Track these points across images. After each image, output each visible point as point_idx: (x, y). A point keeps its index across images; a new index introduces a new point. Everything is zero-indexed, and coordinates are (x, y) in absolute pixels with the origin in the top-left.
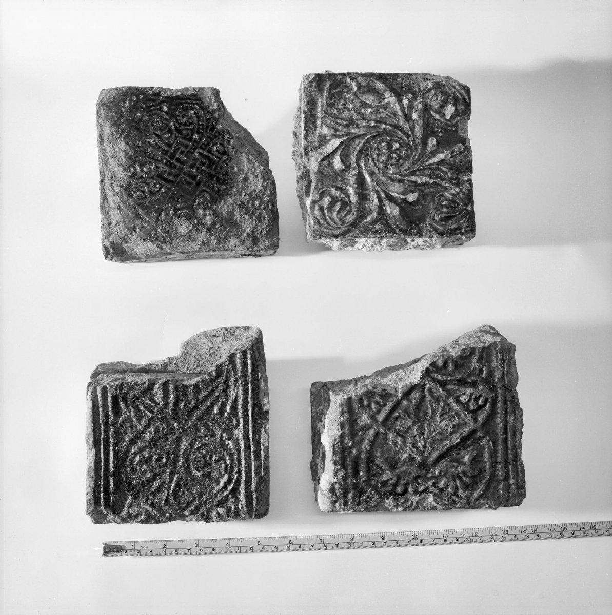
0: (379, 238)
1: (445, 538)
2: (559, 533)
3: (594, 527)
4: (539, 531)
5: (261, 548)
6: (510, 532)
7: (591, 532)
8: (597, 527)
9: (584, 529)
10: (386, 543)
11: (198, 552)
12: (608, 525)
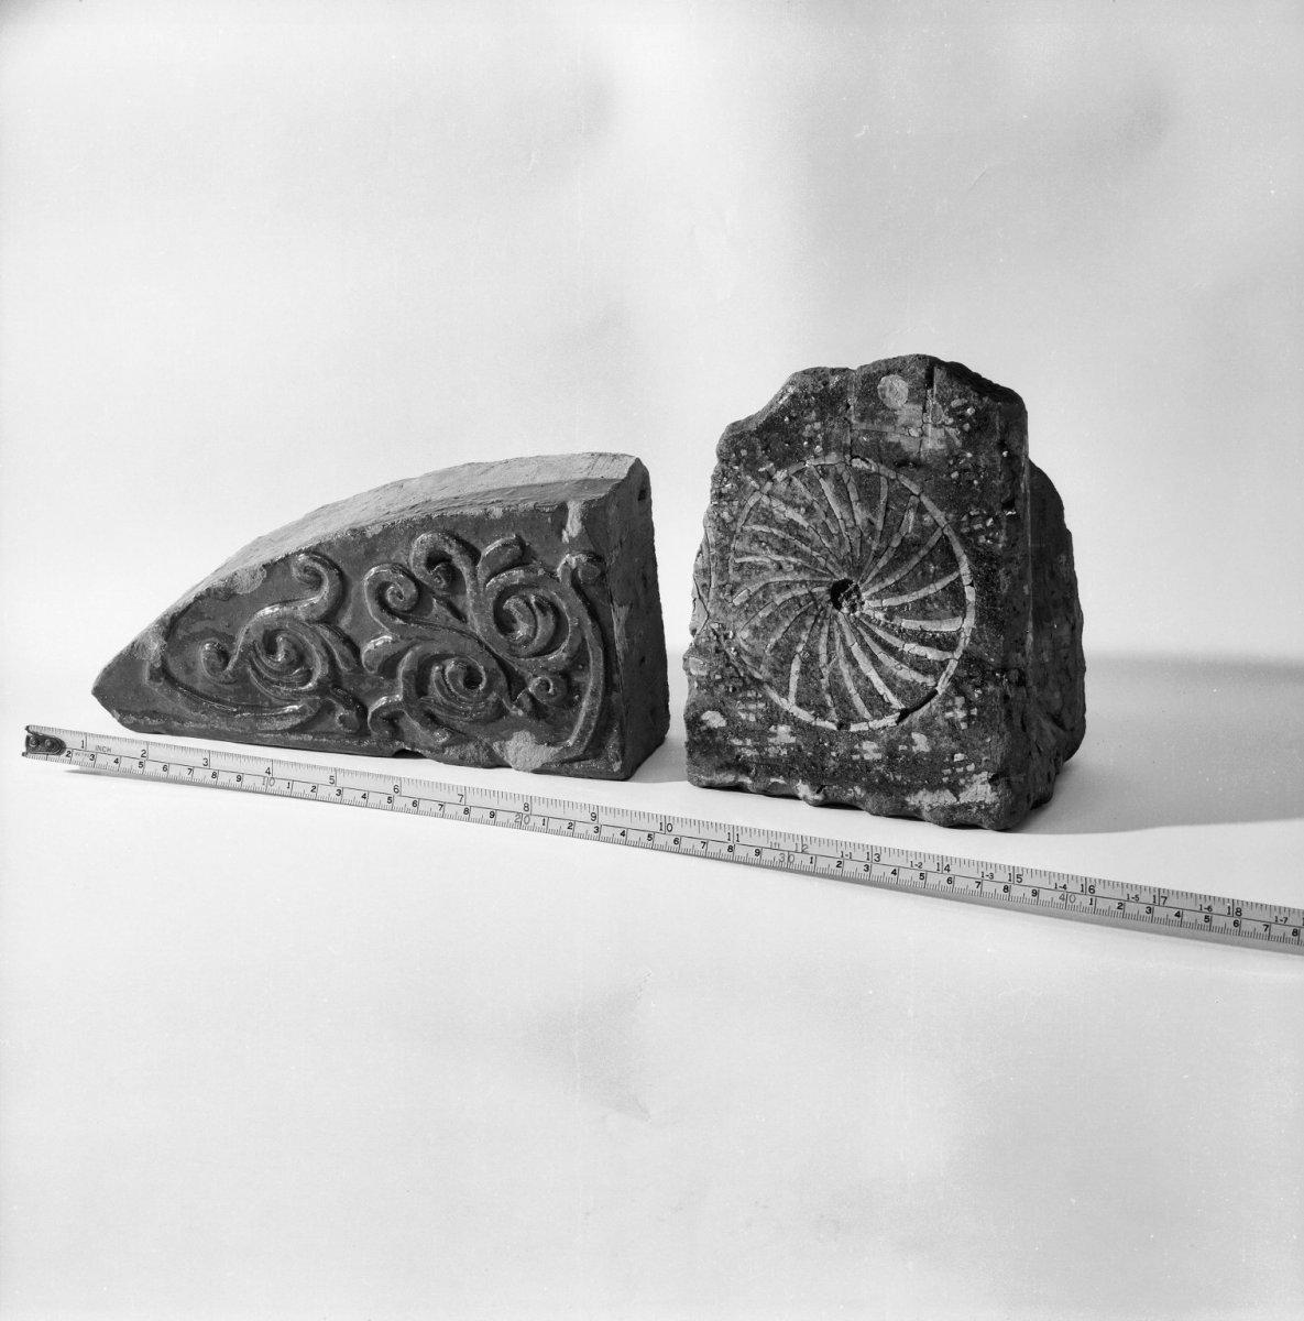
0: (871, 523)
1: (731, 843)
2: (1003, 885)
3: (1092, 889)
4: (954, 870)
5: (333, 791)
6: (1026, 880)
7: (1080, 898)
8: (1099, 891)
9: (1065, 887)
10: (598, 830)
11: (1084, 904)
12: (1127, 891)
